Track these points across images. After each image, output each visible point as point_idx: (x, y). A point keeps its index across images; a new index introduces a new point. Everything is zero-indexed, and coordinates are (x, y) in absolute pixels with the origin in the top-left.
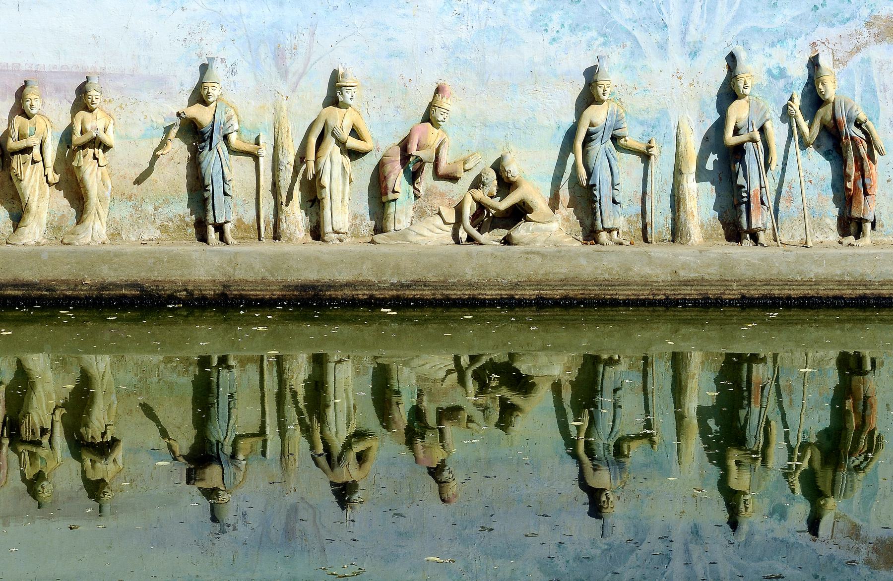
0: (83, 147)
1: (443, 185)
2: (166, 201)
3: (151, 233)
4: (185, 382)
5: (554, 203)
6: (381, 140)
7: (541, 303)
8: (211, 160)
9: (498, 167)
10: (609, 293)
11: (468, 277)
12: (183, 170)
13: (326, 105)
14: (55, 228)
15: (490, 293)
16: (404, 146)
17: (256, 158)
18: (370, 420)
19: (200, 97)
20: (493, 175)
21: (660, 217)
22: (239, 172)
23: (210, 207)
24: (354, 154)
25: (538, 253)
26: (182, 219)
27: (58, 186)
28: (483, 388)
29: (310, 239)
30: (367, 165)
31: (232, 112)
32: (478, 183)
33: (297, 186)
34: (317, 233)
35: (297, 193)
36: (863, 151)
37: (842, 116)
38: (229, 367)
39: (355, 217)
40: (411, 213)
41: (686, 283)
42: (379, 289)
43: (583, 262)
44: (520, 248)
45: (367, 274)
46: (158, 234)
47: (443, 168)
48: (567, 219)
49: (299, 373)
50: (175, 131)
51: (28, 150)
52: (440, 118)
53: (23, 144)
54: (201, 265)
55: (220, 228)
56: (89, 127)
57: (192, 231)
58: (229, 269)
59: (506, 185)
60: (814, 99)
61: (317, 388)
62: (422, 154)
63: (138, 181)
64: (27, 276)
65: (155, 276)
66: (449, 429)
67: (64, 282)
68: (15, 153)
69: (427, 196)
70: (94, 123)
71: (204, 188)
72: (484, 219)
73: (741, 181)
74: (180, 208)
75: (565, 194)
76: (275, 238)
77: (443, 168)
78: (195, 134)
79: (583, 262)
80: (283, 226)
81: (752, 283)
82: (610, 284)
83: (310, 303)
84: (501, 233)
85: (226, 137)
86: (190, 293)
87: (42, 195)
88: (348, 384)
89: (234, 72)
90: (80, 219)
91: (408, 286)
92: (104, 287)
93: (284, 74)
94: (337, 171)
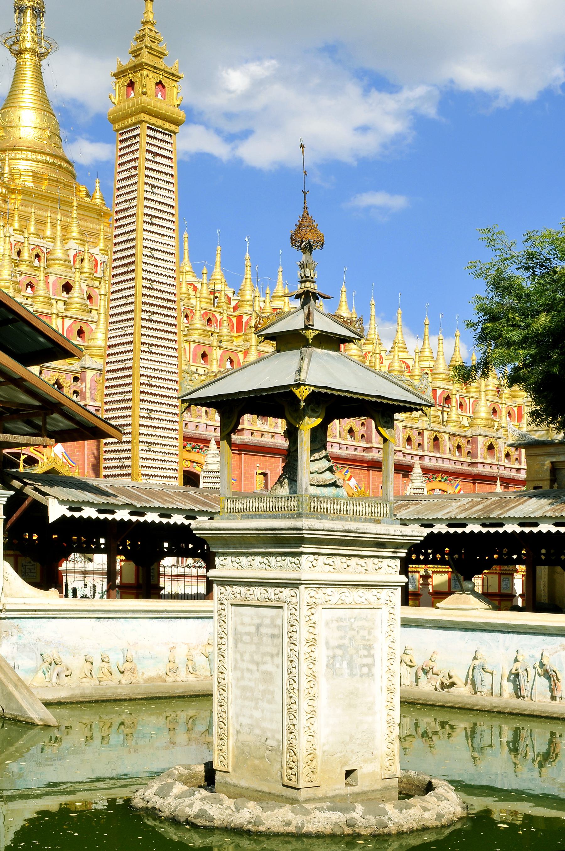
5: (466, 684)
6: (418, 662)
7: (459, 708)
10: (472, 707)
21: (496, 690)
24: (411, 666)
30: (414, 669)
36: (555, 678)
37: (548, 669)
41: (495, 707)
59: (450, 677)
60: (542, 665)
72: (443, 686)
73: (517, 683)
81: (514, 709)
82: (473, 705)
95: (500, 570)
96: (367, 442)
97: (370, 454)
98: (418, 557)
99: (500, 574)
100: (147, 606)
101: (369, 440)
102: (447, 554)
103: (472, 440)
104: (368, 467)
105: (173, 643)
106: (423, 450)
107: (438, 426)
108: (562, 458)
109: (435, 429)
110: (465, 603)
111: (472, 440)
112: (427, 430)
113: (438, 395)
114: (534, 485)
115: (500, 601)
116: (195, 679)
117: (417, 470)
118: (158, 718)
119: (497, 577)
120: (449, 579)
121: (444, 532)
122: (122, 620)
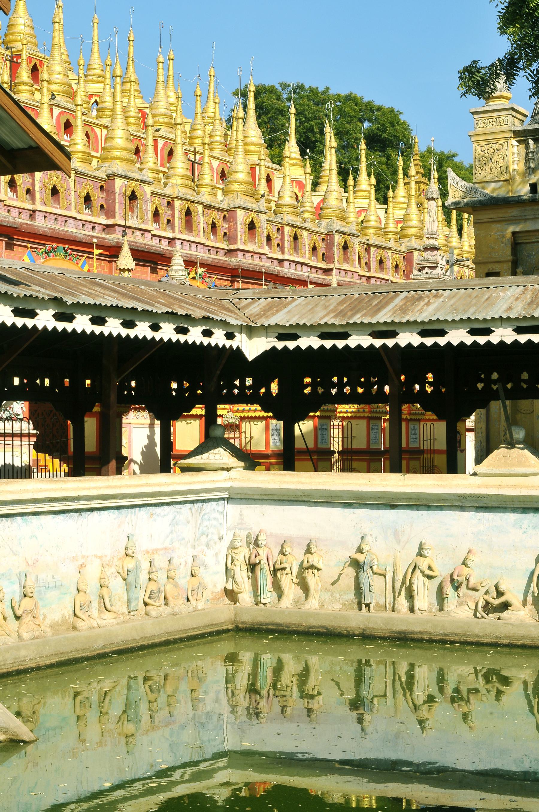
0: (308, 568)
1: (471, 592)
2: (345, 593)
3: (338, 606)
4: (351, 670)
5: (524, 603)
6: (442, 571)
7: (524, 647)
8: (363, 577)
9: (496, 586)
11: (476, 633)
12: (352, 580)
13: (305, 554)
14: (296, 602)
15: (486, 640)
16: (452, 575)
17: (385, 577)
18: (434, 690)
19: (360, 550)
20: (494, 589)
22: (377, 583)
23: (363, 596)
24: (430, 577)
25: (511, 624)
26: (352, 601)
27: (298, 584)
28: (488, 682)
29: (409, 612)
30: (436, 583)
31: (374, 557)
32: (487, 593)
33: (403, 589)
34: (412, 610)
35: (403, 593)
38: (370, 666)
39: (430, 604)
40: (456, 603)
42: (434, 635)
43: (533, 629)
44: (503, 621)
45: (429, 628)
46: (341, 606)
47: (471, 584)
48: (531, 610)
49: (403, 669)
50: (348, 564)
51: (284, 569)
52: (469, 563)
53: (282, 566)
54: (356, 620)
55: (368, 605)
56: (310, 560)
57: (356, 606)
58: (367, 623)
59: (500, 594)
61: (411, 677)
62: (460, 579)
63: (333, 584)
64: (278, 620)
65: (333, 624)
66: (472, 697)
67: (294, 624)
68: (278, 570)
69: (463, 597)
70: (313, 559)
71: (361, 588)
72: (488, 608)
74: (351, 596)
75: (530, 599)
76: (393, 611)
77: (471, 584)
78: (357, 565)
79: (533, 629)
80: (396, 606)
83: (402, 640)
84: (497, 615)
85: (371, 567)
86: (348, 632)
87: (290, 588)
88: (425, 675)
89: (376, 540)
90: (306, 599)
91: (448, 635)
92: (311, 627)
93: (398, 542)
94: (421, 584)
95: (370, 412)
96: (108, 218)
97: (113, 236)
98: (354, 390)
99: (369, 419)
100: (56, 490)
101: (110, 214)
102: (430, 384)
103: (229, 215)
104: (110, 256)
105: (83, 557)
106: (174, 231)
107: (191, 192)
108: (529, 226)
109: (188, 197)
110: (520, 464)
111: (229, 215)
112: (179, 198)
113: (160, 146)
114: (486, 271)
115: (369, 462)
116: (115, 621)
117: (178, 262)
118: (63, 698)
119: (364, 422)
120: (315, 428)
121: (509, 341)
122: (19, 519)
